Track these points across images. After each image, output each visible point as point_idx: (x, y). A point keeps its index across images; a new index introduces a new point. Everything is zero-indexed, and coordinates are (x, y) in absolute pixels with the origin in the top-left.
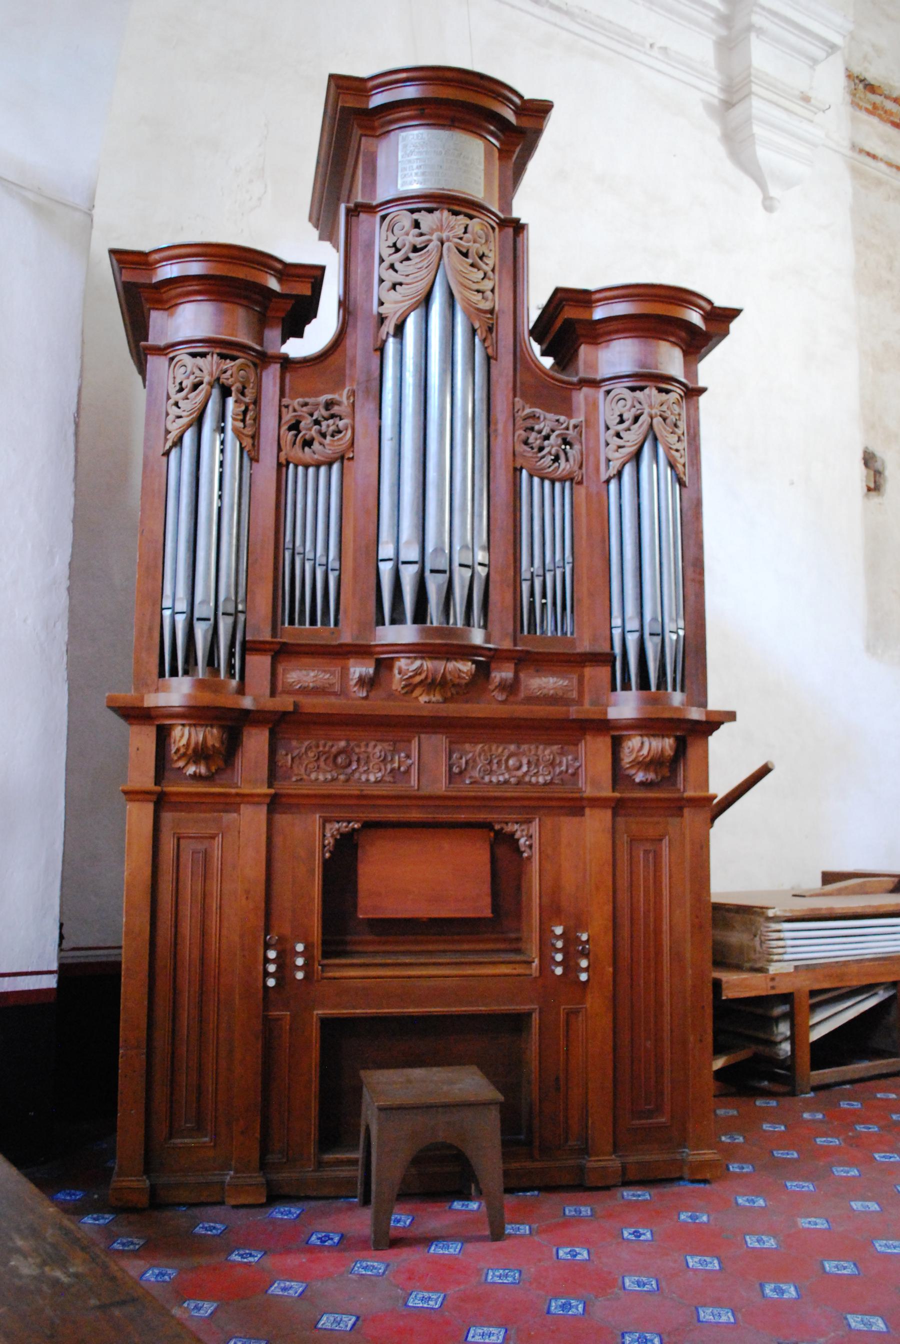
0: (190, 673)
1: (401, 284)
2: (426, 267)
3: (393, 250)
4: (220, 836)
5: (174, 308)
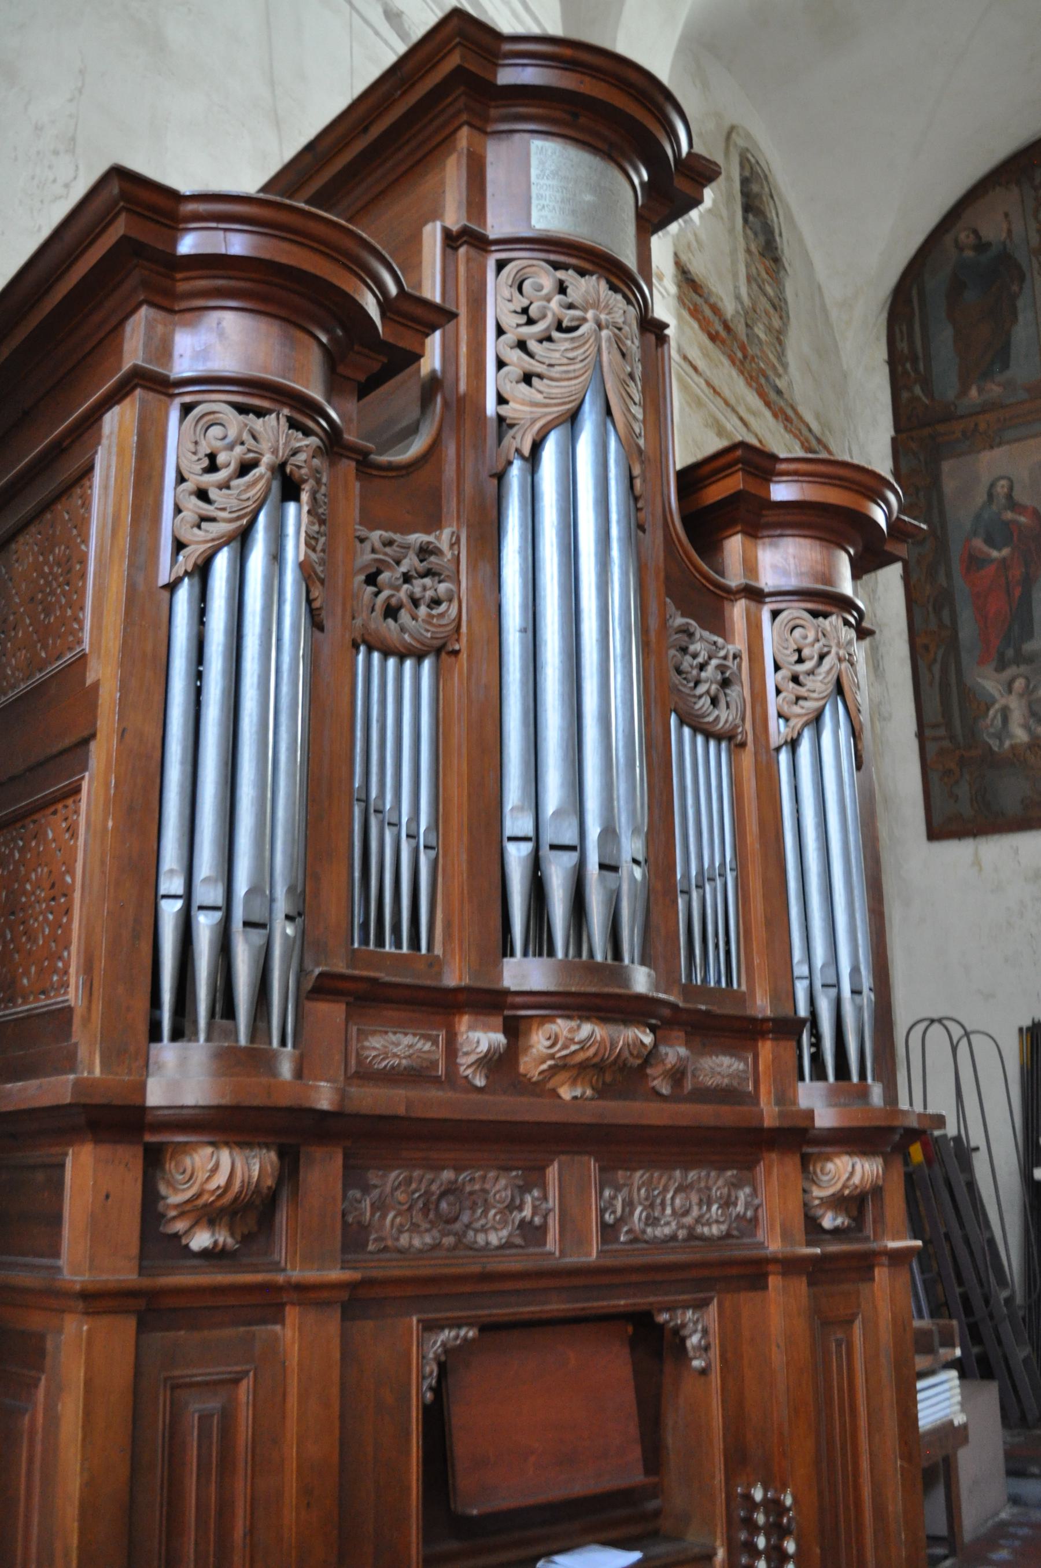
0: (187, 1032)
1: (540, 376)
2: (582, 361)
3: (523, 319)
4: (251, 1374)
5: (197, 313)
